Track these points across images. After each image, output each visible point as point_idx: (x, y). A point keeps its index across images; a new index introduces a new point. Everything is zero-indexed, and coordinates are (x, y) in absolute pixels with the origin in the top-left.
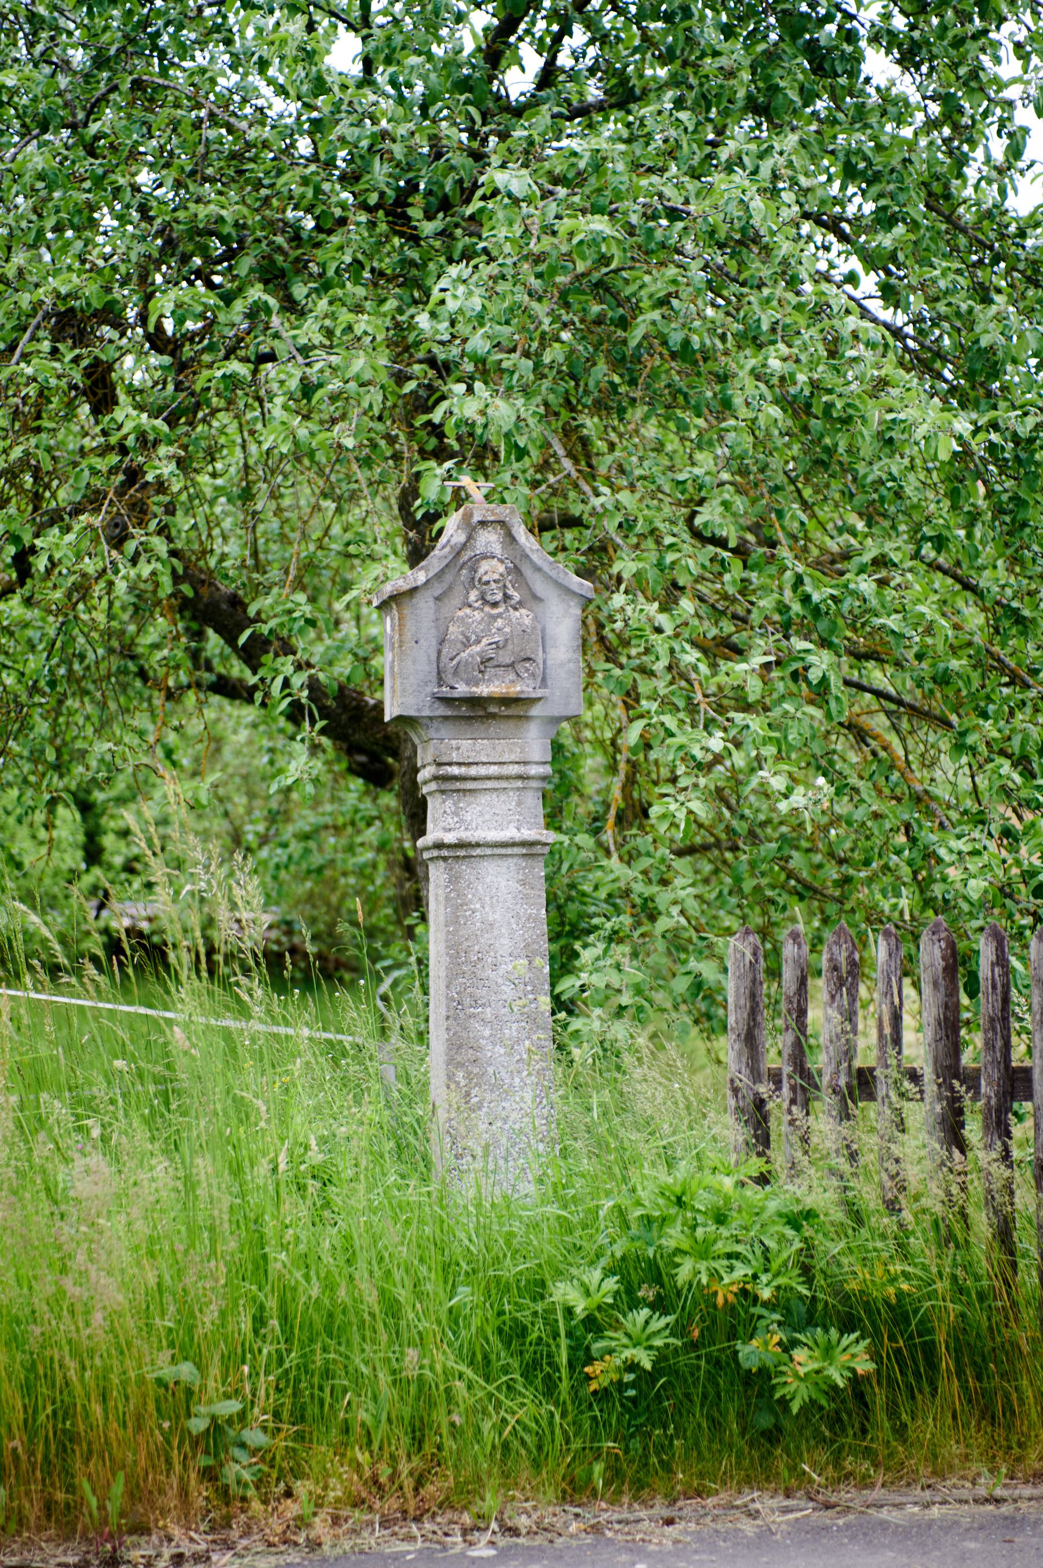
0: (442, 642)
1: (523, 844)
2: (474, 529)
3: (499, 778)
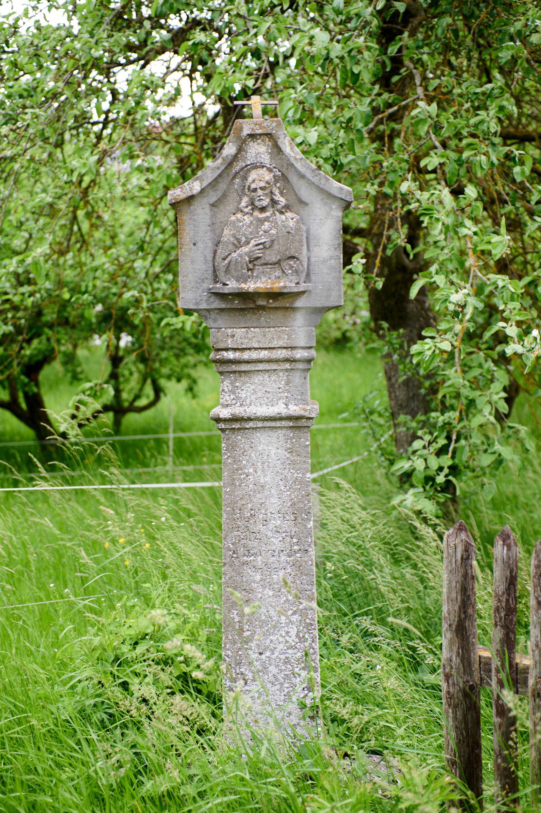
0: (217, 244)
1: (290, 418)
2: (244, 141)
3: (269, 361)
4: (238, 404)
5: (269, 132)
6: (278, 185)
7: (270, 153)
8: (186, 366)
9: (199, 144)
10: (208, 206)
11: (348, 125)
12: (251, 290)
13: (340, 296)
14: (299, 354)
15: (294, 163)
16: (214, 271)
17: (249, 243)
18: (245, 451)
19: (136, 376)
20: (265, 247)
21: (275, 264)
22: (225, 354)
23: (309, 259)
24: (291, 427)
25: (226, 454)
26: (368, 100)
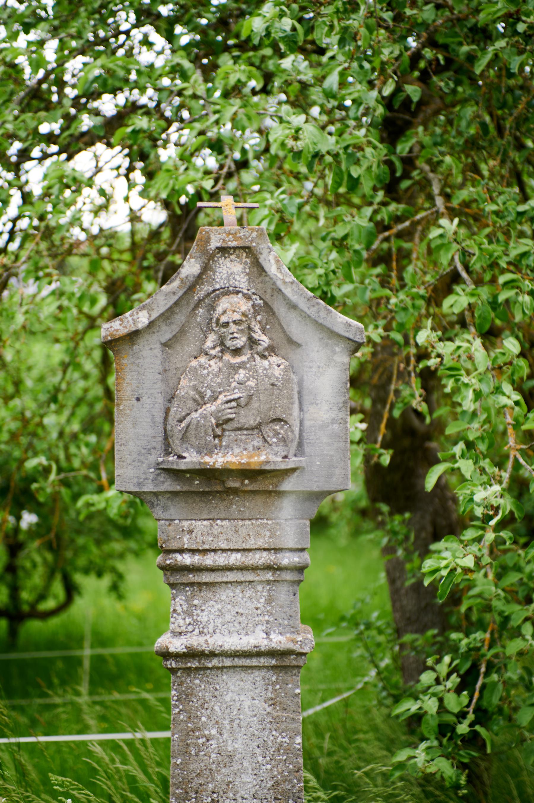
1: (272, 653)
2: (212, 257)
3: (243, 568)
4: (196, 632)
5: (248, 244)
6: (259, 318)
7: (248, 274)
8: (110, 556)
9: (137, 263)
10: (158, 346)
11: (340, 244)
12: (218, 466)
13: (346, 475)
14: (287, 559)
15: (282, 288)
16: (166, 438)
17: (216, 399)
18: (206, 702)
19: (41, 570)
20: (239, 405)
21: (252, 429)
22: (179, 557)
23: (301, 422)
24: (273, 668)
25: (176, 706)
26: (368, 211)
